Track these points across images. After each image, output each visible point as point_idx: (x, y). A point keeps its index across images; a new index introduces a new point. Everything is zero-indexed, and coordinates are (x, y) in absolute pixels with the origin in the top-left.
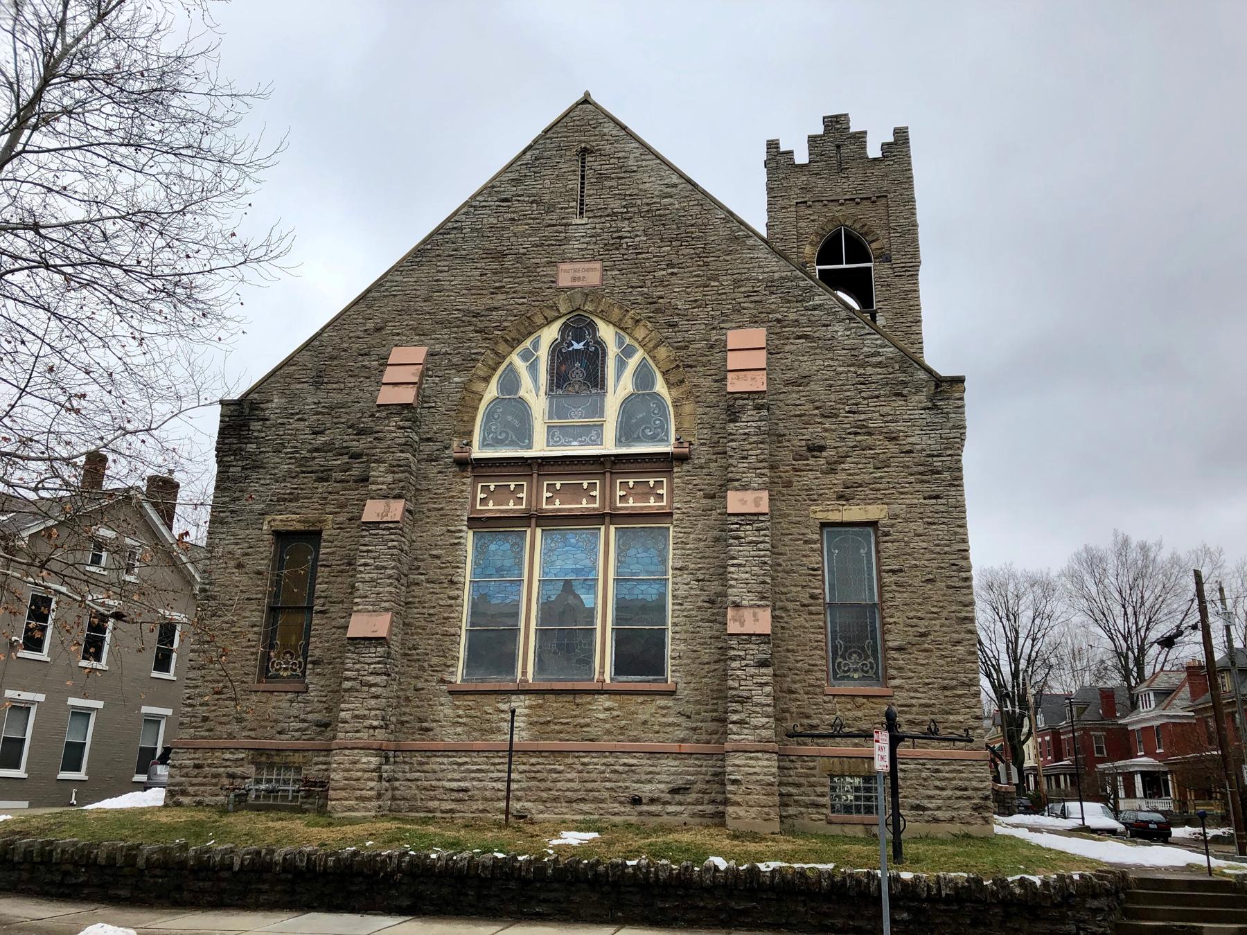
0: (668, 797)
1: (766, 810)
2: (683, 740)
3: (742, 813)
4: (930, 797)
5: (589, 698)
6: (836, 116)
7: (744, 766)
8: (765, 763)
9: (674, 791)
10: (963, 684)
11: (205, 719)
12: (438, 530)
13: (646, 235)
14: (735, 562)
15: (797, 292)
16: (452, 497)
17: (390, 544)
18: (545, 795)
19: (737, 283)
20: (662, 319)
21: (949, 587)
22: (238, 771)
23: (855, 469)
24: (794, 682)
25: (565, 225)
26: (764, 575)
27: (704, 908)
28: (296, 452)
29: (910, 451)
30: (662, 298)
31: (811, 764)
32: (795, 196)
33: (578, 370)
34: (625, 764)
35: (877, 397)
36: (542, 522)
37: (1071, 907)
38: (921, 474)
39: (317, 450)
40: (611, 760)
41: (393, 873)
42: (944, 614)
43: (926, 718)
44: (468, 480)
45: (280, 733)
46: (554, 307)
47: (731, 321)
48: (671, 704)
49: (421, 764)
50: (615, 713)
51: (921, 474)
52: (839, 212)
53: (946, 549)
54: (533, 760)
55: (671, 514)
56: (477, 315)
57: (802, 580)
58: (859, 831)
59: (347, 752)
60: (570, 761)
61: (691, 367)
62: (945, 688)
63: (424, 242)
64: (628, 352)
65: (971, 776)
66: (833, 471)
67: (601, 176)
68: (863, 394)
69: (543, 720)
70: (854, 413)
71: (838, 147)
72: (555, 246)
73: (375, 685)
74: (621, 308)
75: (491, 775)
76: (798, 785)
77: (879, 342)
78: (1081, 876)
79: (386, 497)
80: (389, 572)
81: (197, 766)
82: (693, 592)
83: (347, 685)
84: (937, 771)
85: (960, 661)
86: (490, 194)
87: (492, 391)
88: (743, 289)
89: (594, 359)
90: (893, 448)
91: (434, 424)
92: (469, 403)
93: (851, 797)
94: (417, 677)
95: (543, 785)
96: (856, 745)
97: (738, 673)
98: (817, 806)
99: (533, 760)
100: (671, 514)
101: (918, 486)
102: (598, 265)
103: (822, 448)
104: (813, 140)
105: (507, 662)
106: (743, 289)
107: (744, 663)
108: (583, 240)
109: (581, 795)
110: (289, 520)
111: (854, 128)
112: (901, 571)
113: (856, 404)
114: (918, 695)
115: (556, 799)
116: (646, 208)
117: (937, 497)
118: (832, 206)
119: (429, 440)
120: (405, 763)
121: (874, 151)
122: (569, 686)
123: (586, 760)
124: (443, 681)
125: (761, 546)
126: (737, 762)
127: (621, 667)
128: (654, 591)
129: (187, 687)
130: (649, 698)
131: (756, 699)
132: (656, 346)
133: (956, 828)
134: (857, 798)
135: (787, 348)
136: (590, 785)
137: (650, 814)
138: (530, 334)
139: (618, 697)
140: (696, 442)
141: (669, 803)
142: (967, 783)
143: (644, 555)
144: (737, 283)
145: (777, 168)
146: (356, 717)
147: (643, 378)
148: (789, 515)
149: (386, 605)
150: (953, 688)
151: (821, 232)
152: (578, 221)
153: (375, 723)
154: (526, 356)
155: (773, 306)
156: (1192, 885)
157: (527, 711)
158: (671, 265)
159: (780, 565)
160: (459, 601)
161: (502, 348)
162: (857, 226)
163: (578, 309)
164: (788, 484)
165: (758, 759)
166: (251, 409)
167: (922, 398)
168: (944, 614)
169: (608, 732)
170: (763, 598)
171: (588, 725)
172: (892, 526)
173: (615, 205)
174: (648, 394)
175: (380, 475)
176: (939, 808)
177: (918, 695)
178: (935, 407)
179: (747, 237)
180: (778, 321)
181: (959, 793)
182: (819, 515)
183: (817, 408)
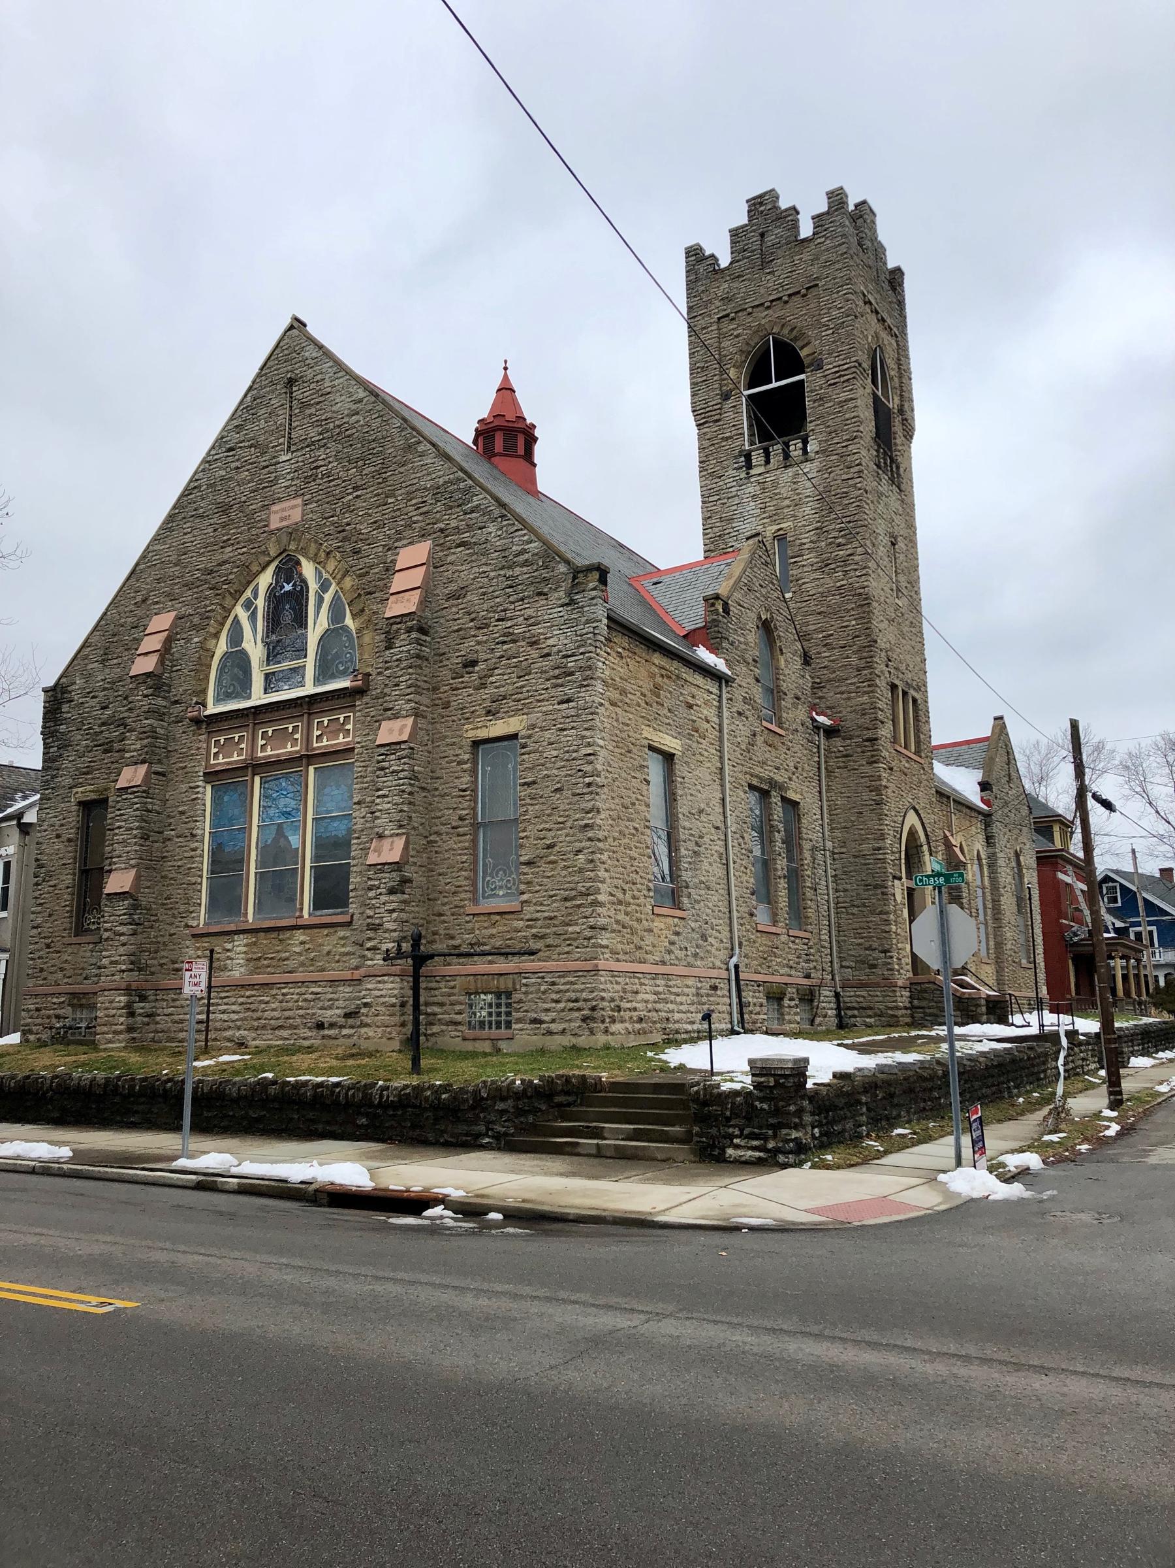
0: (342, 1021)
1: (389, 1029)
2: (357, 968)
3: (371, 1034)
4: (547, 1010)
5: (288, 934)
6: (760, 196)
7: (375, 989)
8: (391, 986)
9: (347, 1016)
10: (582, 894)
11: (42, 970)
12: (184, 787)
13: (337, 460)
14: (380, 793)
15: (457, 496)
16: (192, 755)
17: (135, 806)
18: (256, 1024)
19: (410, 495)
20: (348, 547)
21: (574, 795)
23: (503, 681)
24: (443, 905)
25: (275, 464)
26: (402, 803)
27: (233, 1116)
28: (91, 728)
30: (348, 524)
31: (452, 984)
32: (717, 308)
34: (312, 993)
35: (522, 600)
36: (258, 770)
37: (483, 1110)
38: (556, 677)
39: (103, 724)
40: (303, 990)
41: (44, 1094)
42: (569, 824)
43: (548, 931)
44: (202, 737)
45: (85, 978)
46: (265, 553)
47: (404, 538)
48: (348, 934)
49: (174, 1000)
50: (307, 946)
51: (556, 677)
52: (764, 318)
53: (574, 755)
54: (248, 993)
55: (353, 749)
56: (211, 572)
57: (453, 802)
58: (486, 1047)
59: (106, 993)
60: (274, 992)
61: (370, 593)
62: (566, 899)
63: (174, 507)
64: (324, 587)
65: (583, 986)
66: (483, 686)
67: (304, 405)
68: (511, 599)
69: (255, 956)
70: (503, 620)
71: (762, 235)
73: (123, 934)
74: (316, 542)
75: (220, 1008)
76: (442, 1005)
77: (526, 538)
78: (541, 1078)
79: (136, 763)
80: (135, 832)
81: (38, 1010)
82: (368, 825)
83: (106, 935)
84: (553, 984)
85: (581, 870)
86: (220, 447)
87: (222, 647)
88: (414, 502)
89: (298, 598)
90: (534, 654)
91: (181, 686)
92: (204, 661)
93: (484, 1013)
94: (171, 924)
95: (255, 1015)
96: (490, 962)
97: (374, 901)
98: (456, 1023)
99: (248, 993)
100: (353, 749)
101: (553, 692)
102: (299, 501)
103: (474, 663)
104: (735, 234)
106: (414, 502)
107: (379, 891)
108: (289, 477)
109: (280, 1023)
110: (84, 792)
111: (784, 204)
112: (534, 782)
113: (504, 610)
114: (544, 908)
115: (264, 1027)
116: (338, 430)
117: (568, 701)
118: (761, 314)
119: (176, 702)
120: (163, 1000)
121: (806, 229)
123: (284, 991)
124: (187, 926)
125: (401, 775)
126: (369, 986)
127: (319, 902)
128: (344, 827)
129: (31, 944)
130: (331, 930)
132: (343, 577)
133: (567, 1040)
134: (490, 1014)
136: (287, 1014)
137: (330, 1037)
139: (307, 931)
140: (374, 672)
141: (344, 1027)
142: (578, 994)
143: (336, 792)
144: (410, 495)
145: (697, 280)
146: (112, 962)
147: (336, 614)
148: (446, 737)
149: (132, 862)
150: (573, 898)
151: (745, 348)
152: (284, 458)
153: (124, 967)
154: (248, 605)
155: (438, 515)
156: (657, 1088)
157: (244, 949)
158: (356, 488)
159: (436, 789)
160: (199, 852)
161: (228, 601)
162: (786, 331)
163: (285, 550)
164: (447, 705)
165: (385, 982)
166: (63, 693)
168: (569, 824)
169: (302, 964)
170: (400, 827)
171: (287, 959)
172: (529, 737)
173: (313, 433)
174: (341, 628)
175: (134, 744)
176: (553, 1021)
177: (544, 908)
179: (419, 443)
180: (442, 531)
181: (571, 1005)
182: (470, 734)
183: (472, 620)
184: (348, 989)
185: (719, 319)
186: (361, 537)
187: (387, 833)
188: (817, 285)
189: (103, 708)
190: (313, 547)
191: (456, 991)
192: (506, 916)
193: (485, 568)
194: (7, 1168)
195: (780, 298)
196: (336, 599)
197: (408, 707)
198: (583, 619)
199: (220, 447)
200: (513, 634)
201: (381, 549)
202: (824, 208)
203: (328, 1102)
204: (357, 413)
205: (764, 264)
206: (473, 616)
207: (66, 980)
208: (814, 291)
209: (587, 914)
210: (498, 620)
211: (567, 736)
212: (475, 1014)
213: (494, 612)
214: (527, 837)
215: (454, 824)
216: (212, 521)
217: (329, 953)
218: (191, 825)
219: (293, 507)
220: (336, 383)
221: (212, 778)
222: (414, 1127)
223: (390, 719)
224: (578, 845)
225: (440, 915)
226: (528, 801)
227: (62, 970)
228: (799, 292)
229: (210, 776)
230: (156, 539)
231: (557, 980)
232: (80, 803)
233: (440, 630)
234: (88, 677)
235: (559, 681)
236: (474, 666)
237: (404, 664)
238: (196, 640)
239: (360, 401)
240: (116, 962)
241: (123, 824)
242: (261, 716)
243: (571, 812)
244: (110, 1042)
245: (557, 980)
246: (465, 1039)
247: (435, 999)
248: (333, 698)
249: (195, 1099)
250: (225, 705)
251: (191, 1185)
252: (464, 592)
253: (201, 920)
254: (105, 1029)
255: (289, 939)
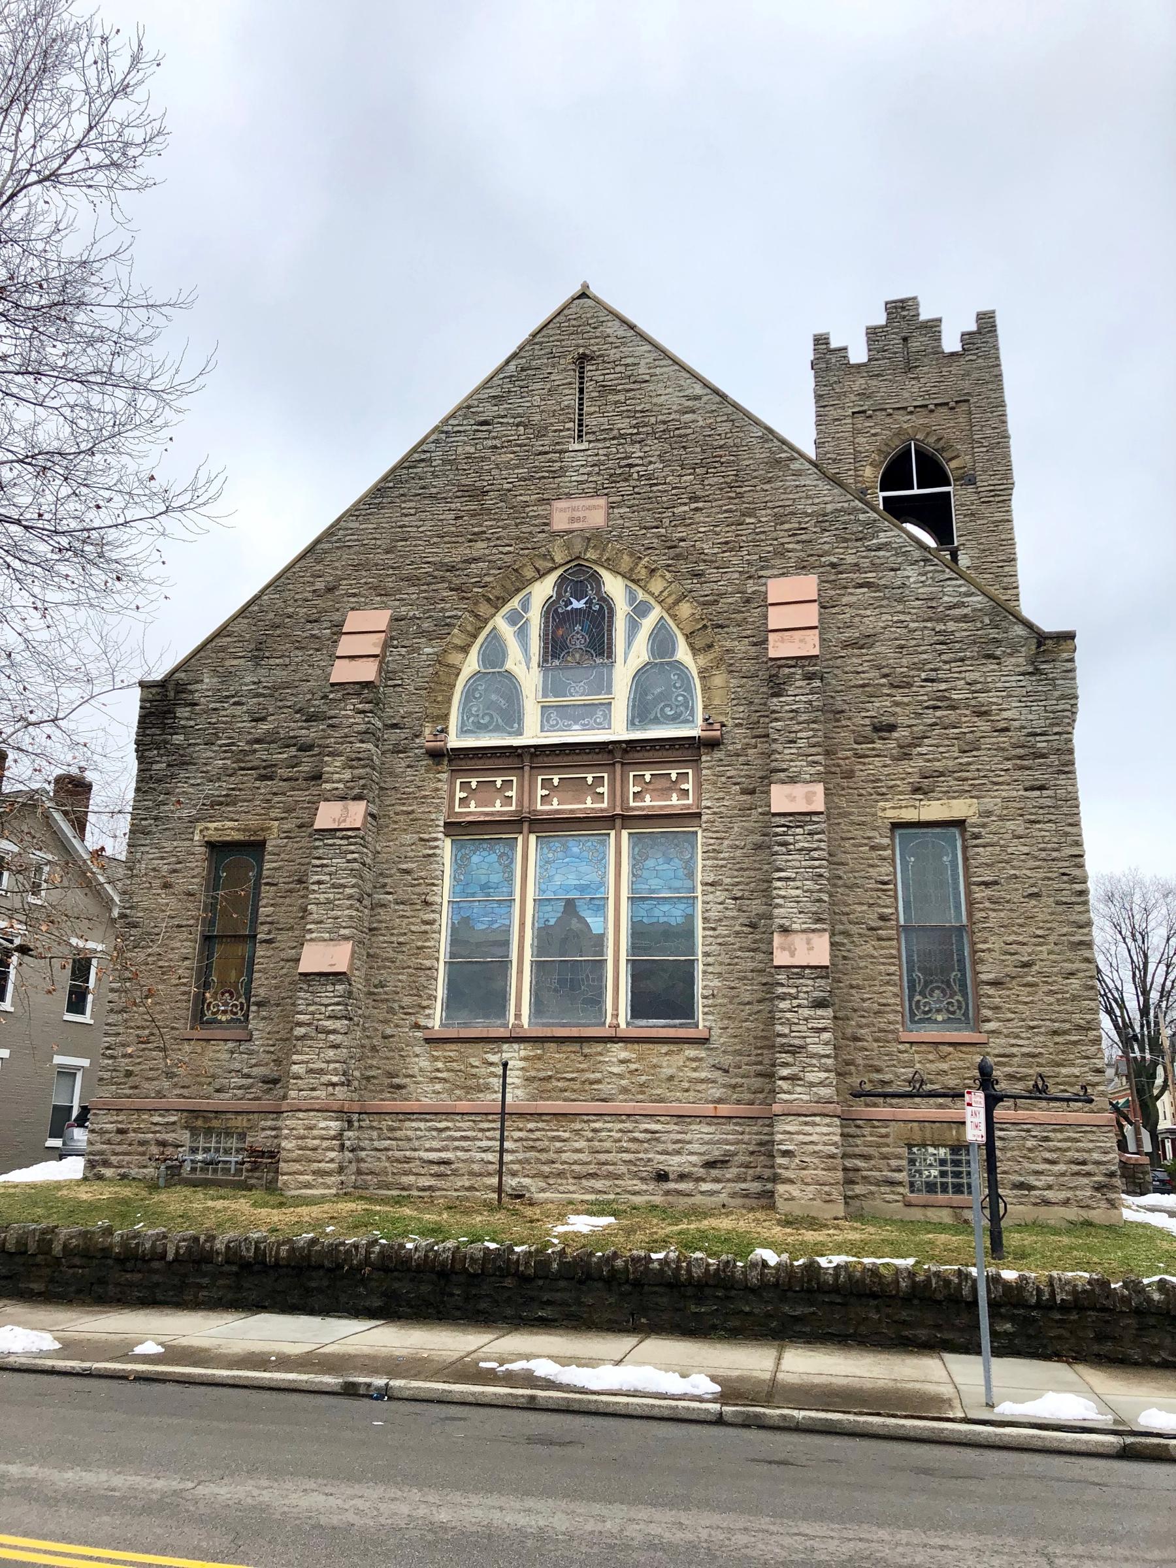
1: (827, 1188)
2: (720, 1101)
4: (1041, 1173)
5: (599, 1048)
6: (902, 301)
7: (798, 1133)
8: (825, 1130)
9: (710, 1165)
10: (1079, 1028)
11: (129, 1074)
12: (408, 838)
13: (662, 461)
14: (782, 874)
16: (425, 797)
18: (546, 1169)
19: (779, 519)
20: (683, 567)
21: (1058, 903)
22: (170, 1137)
23: (935, 753)
25: (561, 452)
26: (820, 891)
28: (233, 744)
29: (1007, 729)
31: (883, 1131)
32: (851, 403)
33: (580, 634)
34: (646, 1131)
35: (962, 660)
36: (537, 827)
38: (1020, 758)
39: (258, 741)
40: (629, 1125)
41: (359, 1269)
42: (1052, 938)
44: (444, 776)
45: (218, 1091)
47: (773, 567)
48: (703, 1054)
50: (633, 1066)
51: (1020, 758)
53: (1055, 854)
54: (531, 1125)
56: (452, 569)
57: (869, 897)
58: (946, 1216)
59: (301, 1115)
60: (578, 1126)
62: (1055, 1033)
63: (385, 479)
64: (641, 610)
65: (1091, 1145)
66: (907, 756)
67: (604, 390)
68: (944, 657)
69: (542, 1074)
70: (933, 681)
71: (905, 339)
72: (548, 480)
73: (334, 1032)
74: (631, 555)
75: (479, 1144)
77: (963, 589)
80: (348, 891)
84: (1046, 1139)
85: (1074, 998)
87: (471, 664)
88: (786, 526)
90: (983, 725)
91: (401, 706)
92: (443, 678)
93: (934, 1172)
95: (544, 1156)
96: (941, 1106)
98: (892, 1183)
99: (531, 1125)
101: (1017, 774)
103: (892, 728)
104: (873, 334)
105: (496, 1002)
106: (786, 526)
108: (582, 470)
109: (592, 1169)
110: (226, 828)
112: (996, 883)
114: (1020, 1042)
115: (560, 1174)
117: (1041, 788)
118: (901, 417)
119: (395, 726)
120: (372, 1128)
122: (574, 1032)
123: (597, 1125)
124: (417, 1026)
125: (815, 854)
126: (788, 1128)
127: (639, 1009)
129: (107, 1034)
130: (673, 1047)
131: (812, 1049)
133: (1072, 1213)
134: (943, 1174)
135: (845, 600)
136: (603, 1157)
137: (679, 1193)
138: (518, 590)
139: (636, 1046)
140: (730, 723)
141: (703, 1180)
144: (779, 519)
146: (311, 1071)
147: (661, 643)
148: (851, 814)
150: (1065, 1033)
151: (884, 448)
153: (335, 1079)
155: (826, 547)
157: (522, 1064)
158: (694, 498)
161: (484, 609)
162: (931, 440)
163: (578, 558)
164: (849, 775)
165: (814, 1124)
166: (177, 692)
167: (1019, 661)
168: (1052, 938)
169: (625, 1090)
170: (819, 920)
171: (599, 1082)
173: (623, 424)
174: (668, 663)
176: (1050, 1187)
177: (1020, 1042)
178: (1037, 671)
179: (793, 459)
182: (890, 813)
184: (706, 1129)
185: (854, 413)
186: (702, 556)
187: (794, 926)
188: (968, 401)
189: (256, 720)
190: (626, 562)
191: (889, 1140)
192: (964, 1049)
193: (902, 617)
194: (260, 1383)
195: (926, 406)
196: (660, 626)
197: (813, 770)
198: (1057, 694)
199: (465, 417)
200: (949, 699)
201: (736, 575)
202: (973, 327)
203: (939, 1297)
204: (693, 412)
205: (909, 369)
206: (886, 671)
207: (178, 1091)
208: (964, 407)
209: (1089, 1053)
210: (926, 680)
211: (1040, 830)
212: (920, 1172)
213: (919, 669)
214: (989, 950)
215: (873, 924)
216: (453, 506)
217: (671, 1078)
218: (422, 889)
219: (595, 507)
220: (658, 371)
221: (453, 831)
222: (1100, 1338)
223: (783, 782)
224: (1068, 966)
225: (856, 1039)
226: (987, 905)
227: (170, 1075)
228: (947, 404)
229: (453, 828)
230: (353, 513)
231: (1051, 1135)
232: (210, 845)
233: (834, 682)
234: (227, 676)
235: (1026, 763)
236: (890, 731)
237: (804, 717)
238: (428, 650)
239: (697, 398)
240: (321, 1072)
241: (327, 878)
242: (540, 759)
243: (1055, 925)
244: (308, 1186)
245: (1051, 1135)
246: (908, 1205)
247: (857, 1150)
248: (653, 748)
249: (993, 1305)
250: (478, 739)
251: (1113, 1451)
252: (870, 640)
253: (436, 1019)
254: (297, 1167)
255: (601, 1054)
